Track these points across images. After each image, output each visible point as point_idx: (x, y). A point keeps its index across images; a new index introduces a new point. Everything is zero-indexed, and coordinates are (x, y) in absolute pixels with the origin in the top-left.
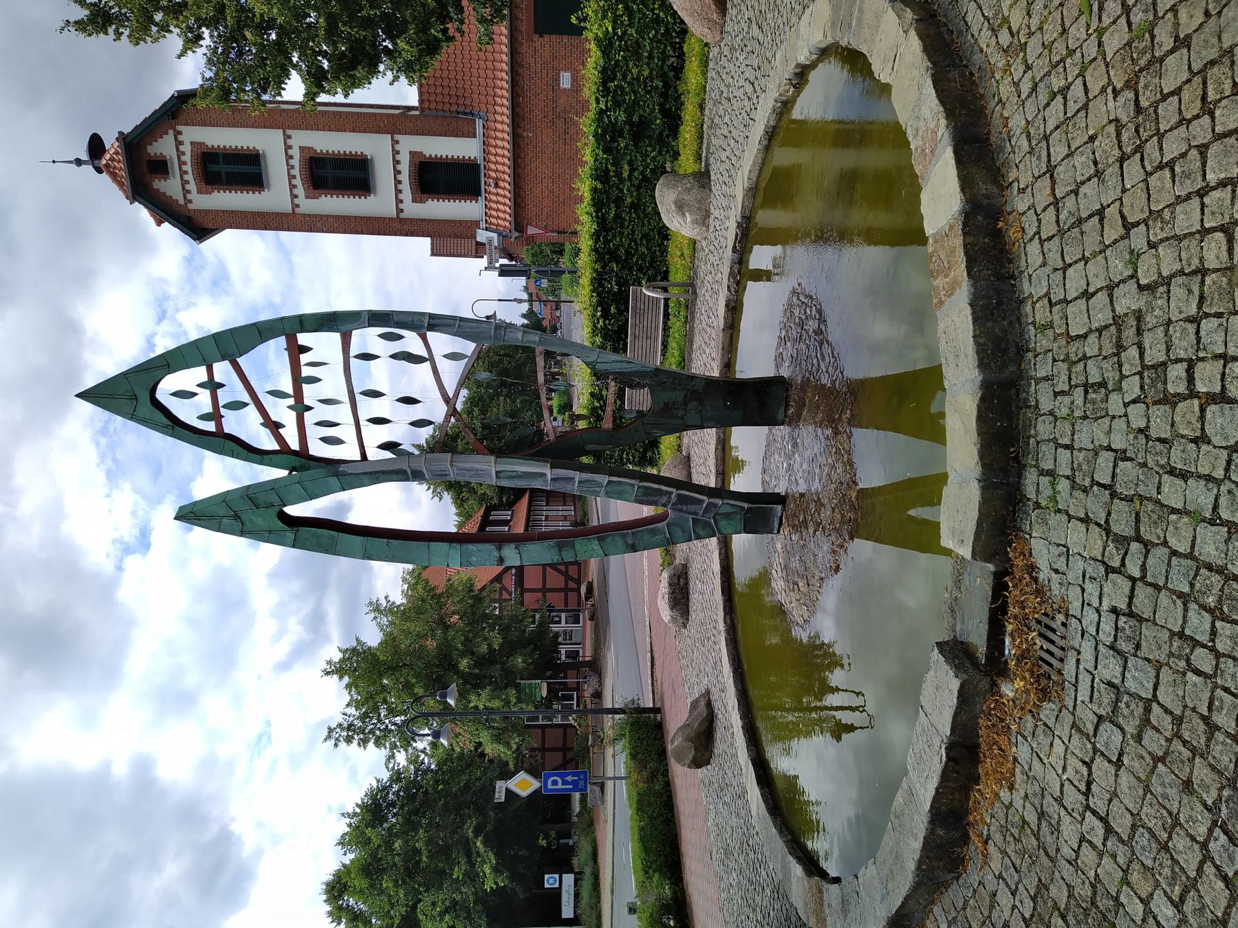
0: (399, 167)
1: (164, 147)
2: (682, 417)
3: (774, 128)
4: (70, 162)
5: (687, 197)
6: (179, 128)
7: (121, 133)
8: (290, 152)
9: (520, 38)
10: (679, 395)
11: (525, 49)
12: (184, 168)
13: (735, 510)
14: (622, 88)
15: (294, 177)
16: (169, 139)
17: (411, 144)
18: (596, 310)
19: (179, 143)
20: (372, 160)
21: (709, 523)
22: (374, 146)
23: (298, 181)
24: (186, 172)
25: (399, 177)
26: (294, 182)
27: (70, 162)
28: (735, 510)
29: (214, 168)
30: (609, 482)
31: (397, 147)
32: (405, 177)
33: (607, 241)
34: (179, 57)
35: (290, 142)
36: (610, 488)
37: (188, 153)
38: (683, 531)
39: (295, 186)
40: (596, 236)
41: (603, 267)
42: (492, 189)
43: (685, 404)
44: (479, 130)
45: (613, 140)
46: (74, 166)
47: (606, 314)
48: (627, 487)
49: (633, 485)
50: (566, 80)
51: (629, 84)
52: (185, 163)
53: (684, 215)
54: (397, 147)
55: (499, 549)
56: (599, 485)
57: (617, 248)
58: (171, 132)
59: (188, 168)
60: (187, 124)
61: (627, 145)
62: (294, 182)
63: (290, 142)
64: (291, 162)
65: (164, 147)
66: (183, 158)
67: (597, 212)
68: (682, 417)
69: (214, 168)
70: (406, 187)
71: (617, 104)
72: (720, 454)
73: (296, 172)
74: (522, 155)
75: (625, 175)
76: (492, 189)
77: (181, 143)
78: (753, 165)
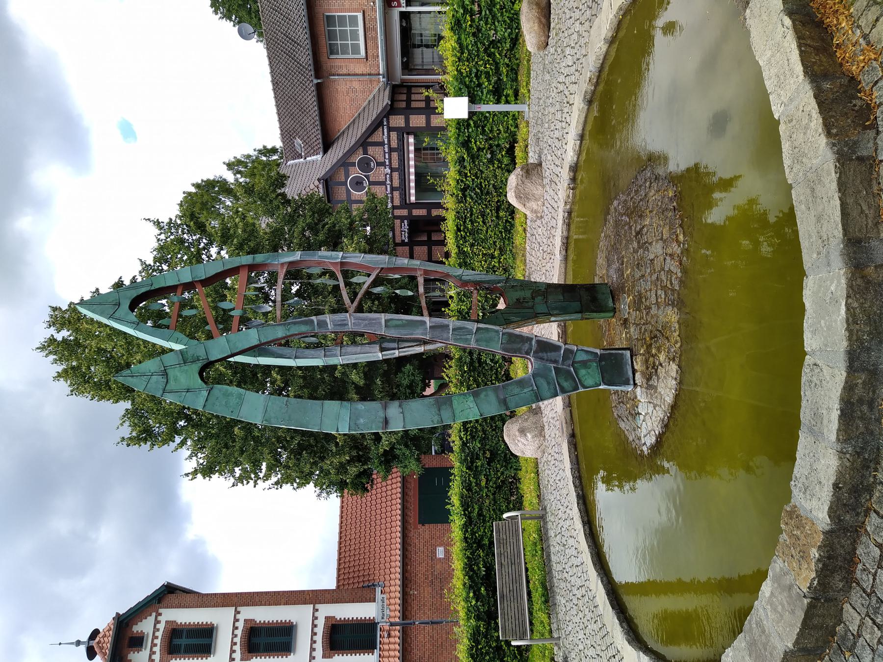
0: (316, 630)
1: (145, 626)
2: (532, 308)
3: (567, 238)
4: (72, 643)
5: (526, 424)
6: (161, 611)
7: (117, 614)
8: (237, 624)
9: (409, 513)
10: (528, 294)
11: (412, 534)
12: (156, 641)
13: (590, 357)
14: (476, 428)
15: (235, 644)
16: (151, 620)
17: (327, 610)
18: (468, 593)
19: (157, 622)
20: (296, 625)
21: (569, 372)
22: (299, 616)
23: (237, 648)
24: (156, 645)
25: (315, 638)
26: (235, 648)
27: (72, 643)
28: (590, 357)
29: (177, 641)
30: (478, 329)
31: (317, 614)
32: (319, 638)
33: (473, 533)
34: (186, 459)
35: (238, 616)
36: (479, 336)
37: (161, 630)
38: (548, 383)
39: (234, 651)
40: (465, 528)
41: (472, 553)
42: (386, 640)
43: (533, 298)
44: (379, 596)
45: (472, 462)
46: (74, 646)
47: (477, 597)
48: (494, 334)
49: (497, 331)
50: (440, 553)
51: (480, 425)
52: (157, 638)
53: (525, 435)
54: (317, 614)
55: (385, 408)
56: (470, 332)
57: (482, 537)
58: (154, 614)
59: (158, 642)
60: (167, 607)
61: (482, 465)
62: (235, 648)
63: (238, 616)
64: (236, 632)
65: (145, 626)
66: (157, 634)
67: (464, 511)
68: (532, 308)
69: (177, 641)
70: (319, 646)
71: (473, 438)
72: (582, 507)
73: (238, 640)
74: (409, 608)
75: (483, 484)
76: (386, 640)
77: (159, 622)
78: (560, 275)
